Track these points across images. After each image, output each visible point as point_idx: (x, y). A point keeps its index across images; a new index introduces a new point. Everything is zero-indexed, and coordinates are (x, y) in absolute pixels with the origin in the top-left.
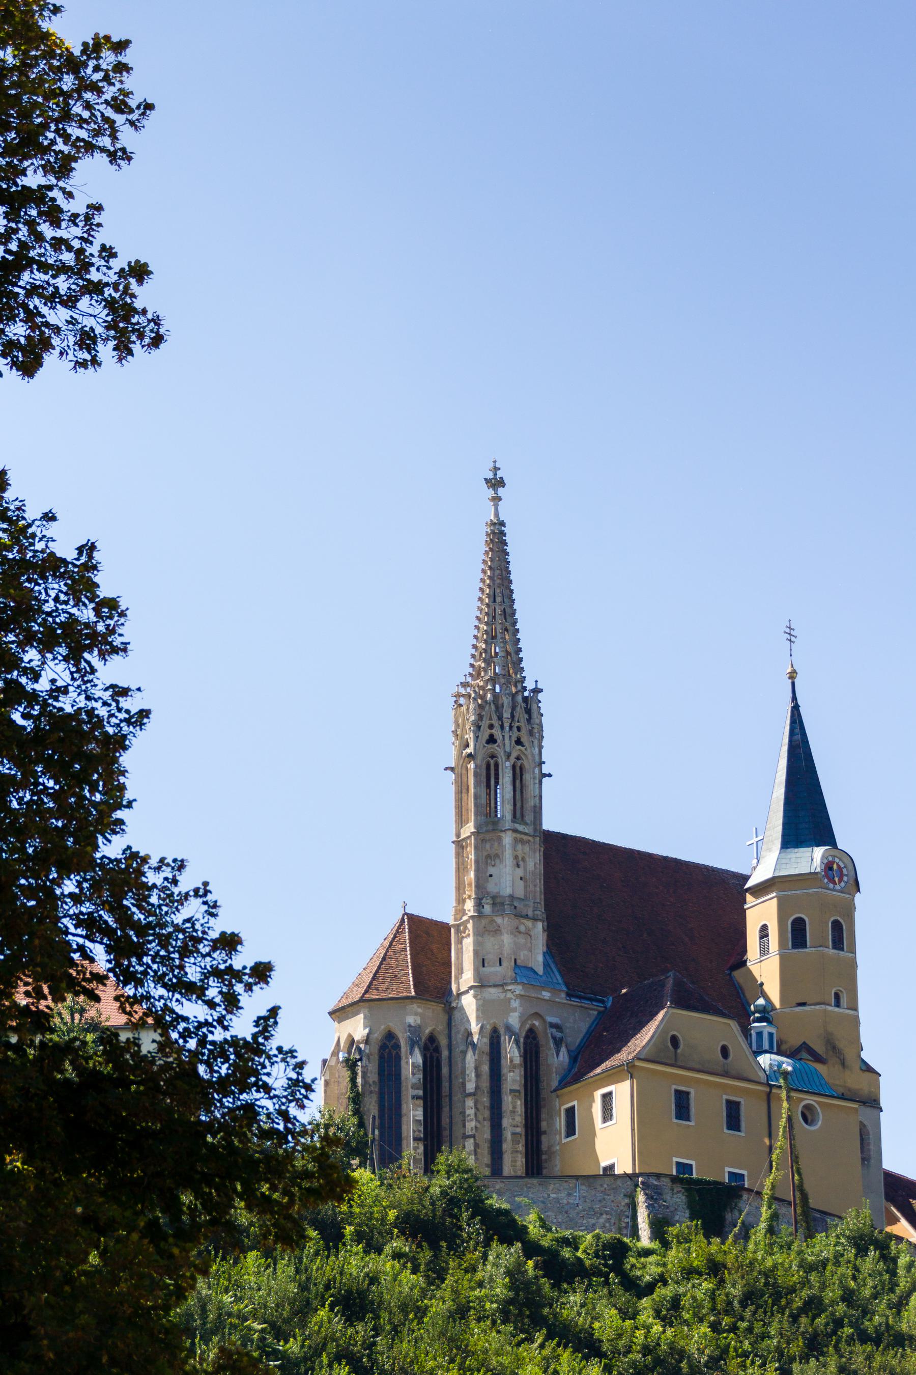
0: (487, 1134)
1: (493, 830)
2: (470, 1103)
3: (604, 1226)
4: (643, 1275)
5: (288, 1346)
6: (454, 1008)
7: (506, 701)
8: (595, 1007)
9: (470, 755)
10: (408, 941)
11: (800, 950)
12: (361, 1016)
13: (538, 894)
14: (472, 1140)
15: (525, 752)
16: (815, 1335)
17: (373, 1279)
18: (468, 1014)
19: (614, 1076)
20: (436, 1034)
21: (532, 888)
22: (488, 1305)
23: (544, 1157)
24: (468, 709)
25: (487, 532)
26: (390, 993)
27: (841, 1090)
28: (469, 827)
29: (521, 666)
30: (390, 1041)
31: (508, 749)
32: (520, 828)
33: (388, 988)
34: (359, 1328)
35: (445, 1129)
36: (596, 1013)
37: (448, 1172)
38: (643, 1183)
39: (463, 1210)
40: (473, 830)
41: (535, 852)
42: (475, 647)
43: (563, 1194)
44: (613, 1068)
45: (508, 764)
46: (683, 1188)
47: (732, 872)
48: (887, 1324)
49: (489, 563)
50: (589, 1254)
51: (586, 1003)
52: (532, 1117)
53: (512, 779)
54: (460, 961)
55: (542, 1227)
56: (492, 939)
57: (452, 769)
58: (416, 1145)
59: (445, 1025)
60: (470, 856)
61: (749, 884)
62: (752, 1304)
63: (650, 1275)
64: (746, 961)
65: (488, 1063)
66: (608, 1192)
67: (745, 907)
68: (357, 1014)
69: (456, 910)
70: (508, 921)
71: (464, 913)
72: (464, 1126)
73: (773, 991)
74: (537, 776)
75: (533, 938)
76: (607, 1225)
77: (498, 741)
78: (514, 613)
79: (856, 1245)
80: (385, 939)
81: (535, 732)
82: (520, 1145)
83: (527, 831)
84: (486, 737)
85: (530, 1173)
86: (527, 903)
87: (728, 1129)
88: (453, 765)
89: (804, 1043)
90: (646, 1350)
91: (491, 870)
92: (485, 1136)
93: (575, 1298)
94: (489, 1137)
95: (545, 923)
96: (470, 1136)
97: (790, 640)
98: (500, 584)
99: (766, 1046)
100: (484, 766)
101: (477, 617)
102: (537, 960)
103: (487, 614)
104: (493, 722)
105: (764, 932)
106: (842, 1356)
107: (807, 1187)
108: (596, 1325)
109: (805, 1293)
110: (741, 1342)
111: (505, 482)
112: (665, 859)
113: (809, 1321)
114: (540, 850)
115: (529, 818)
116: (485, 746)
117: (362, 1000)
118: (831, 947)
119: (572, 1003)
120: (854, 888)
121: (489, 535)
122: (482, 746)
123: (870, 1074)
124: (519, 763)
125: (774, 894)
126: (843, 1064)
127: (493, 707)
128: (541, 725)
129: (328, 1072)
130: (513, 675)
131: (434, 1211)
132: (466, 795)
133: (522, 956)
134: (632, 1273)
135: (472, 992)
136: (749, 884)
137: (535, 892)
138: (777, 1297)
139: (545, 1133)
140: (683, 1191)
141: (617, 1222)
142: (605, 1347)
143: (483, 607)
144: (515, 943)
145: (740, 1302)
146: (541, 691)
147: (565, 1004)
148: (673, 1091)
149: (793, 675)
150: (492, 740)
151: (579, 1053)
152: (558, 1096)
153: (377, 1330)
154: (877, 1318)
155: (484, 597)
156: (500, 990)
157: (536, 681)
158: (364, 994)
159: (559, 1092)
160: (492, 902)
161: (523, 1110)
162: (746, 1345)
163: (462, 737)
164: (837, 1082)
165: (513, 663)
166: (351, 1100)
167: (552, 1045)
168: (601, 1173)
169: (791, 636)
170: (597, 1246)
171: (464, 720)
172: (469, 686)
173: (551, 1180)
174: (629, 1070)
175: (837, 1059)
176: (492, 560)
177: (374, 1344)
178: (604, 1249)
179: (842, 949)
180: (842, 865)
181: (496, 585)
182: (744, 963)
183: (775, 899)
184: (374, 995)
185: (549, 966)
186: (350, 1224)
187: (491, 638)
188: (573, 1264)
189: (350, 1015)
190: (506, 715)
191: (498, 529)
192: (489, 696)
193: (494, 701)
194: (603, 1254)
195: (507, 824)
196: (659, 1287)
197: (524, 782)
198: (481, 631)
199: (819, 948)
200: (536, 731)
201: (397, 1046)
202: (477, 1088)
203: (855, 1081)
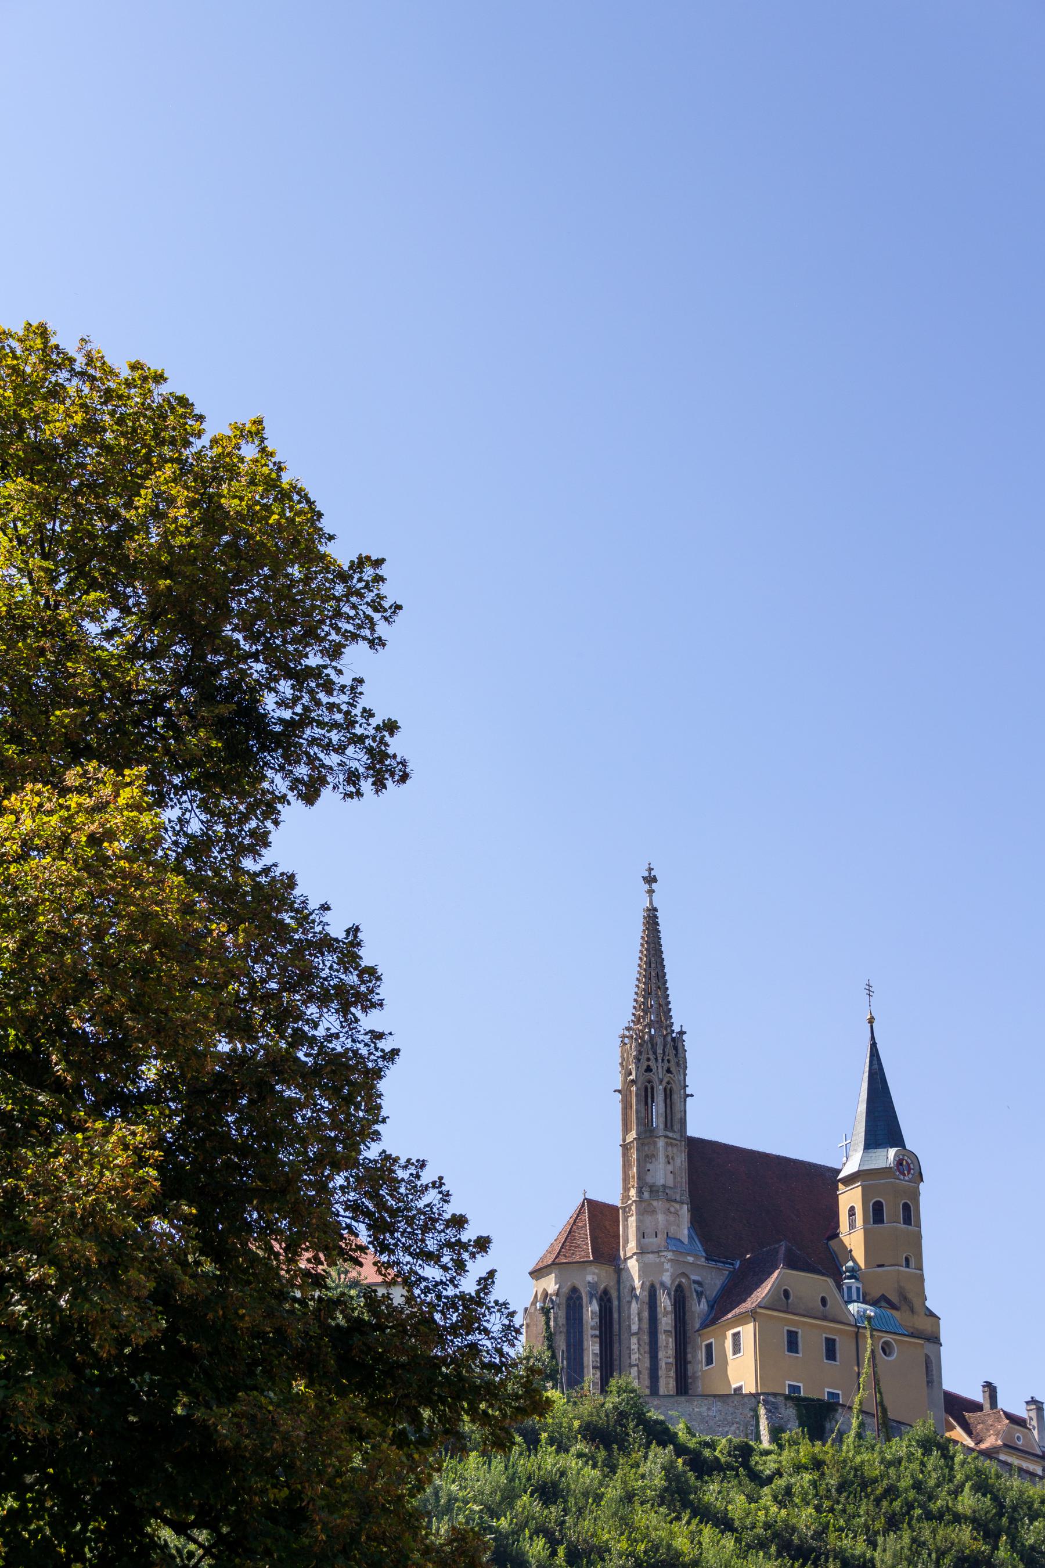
0: (647, 1364)
7: (659, 1041)
9: (632, 1081)
16: (894, 1514)
17: (563, 1474)
19: (741, 1320)
21: (679, 1179)
32: (670, 1134)
34: (553, 1510)
37: (618, 1392)
42: (635, 1000)
43: (704, 1409)
44: (741, 1314)
48: (947, 1507)
57: (619, 1091)
61: (841, 1176)
71: (629, 1199)
78: (664, 975)
81: (681, 1064)
84: (645, 1067)
88: (620, 1088)
90: (767, 1526)
93: (714, 1487)
96: (634, 1365)
99: (855, 1297)
102: (684, 1232)
103: (645, 976)
105: (852, 1211)
107: (886, 1403)
108: (730, 1507)
115: (677, 1127)
117: (554, 1263)
123: (930, 1318)
126: (912, 1311)
131: (608, 1421)
133: (673, 1229)
136: (841, 1176)
138: (864, 1485)
149: (871, 1021)
150: (649, 1069)
154: (939, 1503)
156: (656, 1255)
162: (842, 1522)
165: (664, 1012)
173: (696, 1399)
174: (753, 1315)
176: (647, 936)
177: (564, 1522)
182: (837, 1235)
186: (545, 1432)
187: (647, 994)
188: (711, 1461)
190: (659, 1051)
201: (580, 1298)
202: (639, 1329)
203: (922, 1323)
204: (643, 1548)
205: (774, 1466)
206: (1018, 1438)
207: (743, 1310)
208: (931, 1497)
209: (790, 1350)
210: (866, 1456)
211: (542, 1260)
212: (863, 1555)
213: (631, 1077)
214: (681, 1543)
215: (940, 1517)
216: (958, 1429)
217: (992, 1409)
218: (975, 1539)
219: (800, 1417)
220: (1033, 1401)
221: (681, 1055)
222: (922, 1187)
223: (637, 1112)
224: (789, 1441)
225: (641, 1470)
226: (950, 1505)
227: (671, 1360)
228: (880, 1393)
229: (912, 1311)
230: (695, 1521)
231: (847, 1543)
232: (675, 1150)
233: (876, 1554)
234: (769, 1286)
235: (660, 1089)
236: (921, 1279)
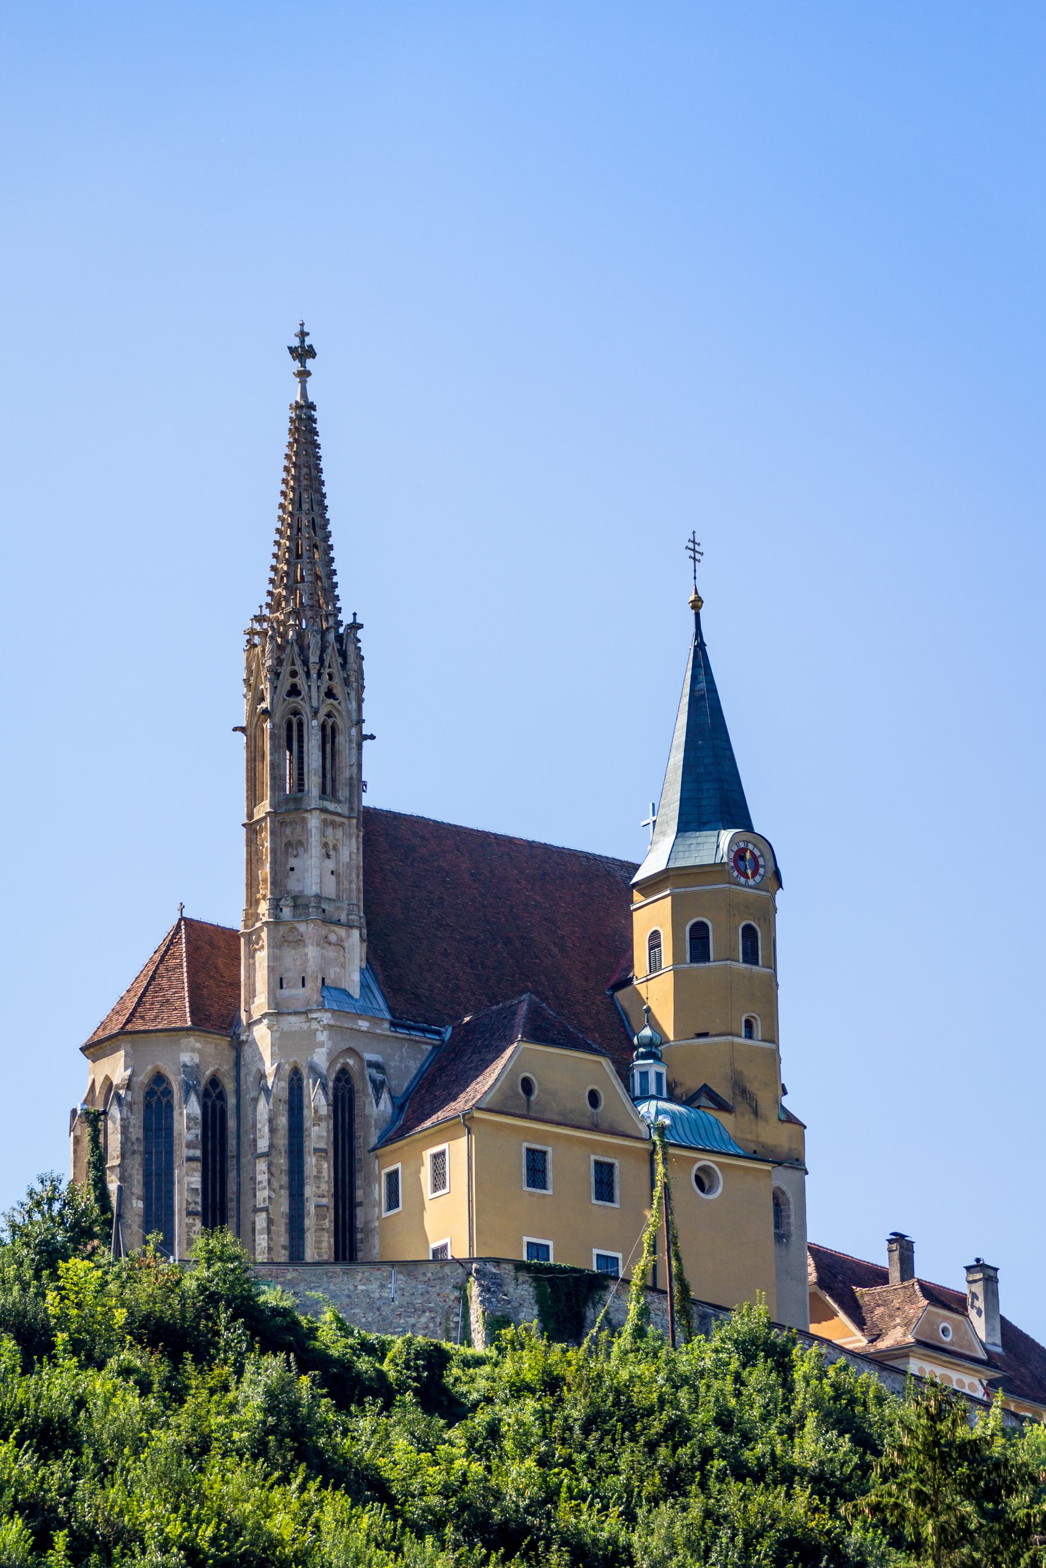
0: (284, 1206)
1: (296, 809)
2: (262, 1166)
3: (427, 1327)
4: (469, 1392)
6: (243, 1042)
7: (313, 641)
8: (429, 1041)
9: (265, 712)
10: (184, 955)
11: (701, 965)
12: (122, 1053)
13: (354, 894)
14: (264, 1215)
15: (339, 707)
16: (679, 1468)
17: (81, 1403)
18: (261, 1050)
19: (446, 1130)
20: (219, 1076)
21: (346, 885)
22: (236, 1436)
23: (359, 1236)
24: (263, 651)
25: (291, 418)
26: (159, 1022)
27: (753, 1147)
28: (264, 806)
29: (336, 593)
30: (159, 1085)
31: (315, 704)
32: (331, 806)
33: (156, 1017)
34: (55, 1468)
35: (232, 1200)
36: (430, 1048)
37: (208, 1260)
39: (222, 1308)
40: (269, 810)
42: (274, 568)
43: (374, 1286)
44: (447, 1120)
46: (530, 1277)
47: (621, 861)
48: (773, 1454)
50: (397, 1365)
51: (416, 1035)
52: (344, 1186)
53: (320, 742)
54: (251, 980)
55: (340, 1329)
56: (293, 952)
57: (243, 730)
58: (191, 1221)
59: (232, 1063)
60: (266, 844)
61: (638, 877)
62: (598, 1429)
63: (478, 1392)
64: (633, 978)
65: (286, 1115)
66: (432, 1283)
67: (632, 908)
68: (118, 1050)
70: (314, 929)
71: (258, 919)
72: (255, 1196)
74: (354, 738)
75: (346, 950)
76: (431, 1325)
77: (303, 693)
79: (745, 1352)
80: (155, 952)
81: (354, 682)
82: (327, 1220)
83: (340, 811)
84: (287, 687)
85: (341, 1257)
87: (597, 1199)
88: (244, 724)
89: (705, 1085)
90: (447, 1491)
91: (292, 862)
92: (282, 1210)
93: (365, 1424)
94: (287, 1210)
95: (365, 931)
96: (262, 1210)
97: (694, 559)
98: (307, 486)
99: (653, 1090)
100: (284, 726)
102: (353, 979)
103: (290, 526)
104: (296, 668)
106: (709, 1497)
107: (687, 1276)
109: (668, 1414)
110: (577, 1480)
111: (316, 351)
112: (531, 845)
113: (670, 1452)
114: (358, 837)
115: (343, 793)
117: (123, 1032)
118: (741, 961)
119: (398, 1035)
120: (773, 883)
122: (281, 699)
123: (791, 1126)
124: (330, 721)
126: (756, 1113)
127: (296, 648)
128: (360, 672)
130: (324, 607)
131: (183, 1311)
132: (261, 764)
133: (333, 974)
134: (456, 1389)
135: (265, 1021)
136: (638, 877)
138: (629, 1422)
139: (360, 1204)
140: (530, 1280)
141: (443, 1321)
142: (395, 1489)
143: (286, 516)
144: (323, 957)
146: (361, 626)
148: (524, 1150)
149: (697, 604)
150: (294, 691)
151: (405, 1102)
152: (377, 1157)
153: (77, 1472)
154: (760, 1448)
155: (286, 503)
156: (303, 1018)
157: (355, 614)
158: (126, 1024)
159: (379, 1152)
160: (292, 904)
161: (332, 1175)
162: (585, 1484)
163: (256, 687)
164: (748, 1137)
165: (324, 590)
166: (92, 1165)
167: (370, 1090)
168: (431, 1258)
169: (695, 552)
170: (408, 1354)
171: (258, 666)
172: (265, 621)
174: (467, 1122)
175: (748, 1107)
176: (296, 454)
177: (73, 1489)
178: (417, 1358)
179: (756, 963)
180: (757, 853)
181: (303, 487)
182: (628, 982)
184: (138, 1025)
185: (369, 987)
186: (62, 1331)
187: (295, 555)
189: (108, 1052)
190: (314, 658)
191: (305, 414)
193: (297, 641)
194: (415, 1364)
195: (313, 802)
196: (482, 1408)
197: (337, 747)
198: (283, 548)
199: (725, 962)
200: (353, 679)
201: (168, 1092)
202: (271, 1146)
203: (773, 1135)
204: (209, 1533)
205: (482, 1384)
208: (747, 1439)
210: (644, 1369)
211: (103, 1025)
212: (613, 1540)
213: (264, 705)
215: (758, 1477)
216: (842, 1316)
217: (903, 1280)
219: (540, 1300)
220: (979, 1266)
221: (352, 664)
222: (781, 897)
224: (512, 1342)
226: (779, 1450)
228: (678, 1259)
229: (756, 1113)
230: (313, 1486)
231: (587, 1519)
232: (339, 833)
233: (635, 1538)
235: (314, 725)
236: (774, 1059)
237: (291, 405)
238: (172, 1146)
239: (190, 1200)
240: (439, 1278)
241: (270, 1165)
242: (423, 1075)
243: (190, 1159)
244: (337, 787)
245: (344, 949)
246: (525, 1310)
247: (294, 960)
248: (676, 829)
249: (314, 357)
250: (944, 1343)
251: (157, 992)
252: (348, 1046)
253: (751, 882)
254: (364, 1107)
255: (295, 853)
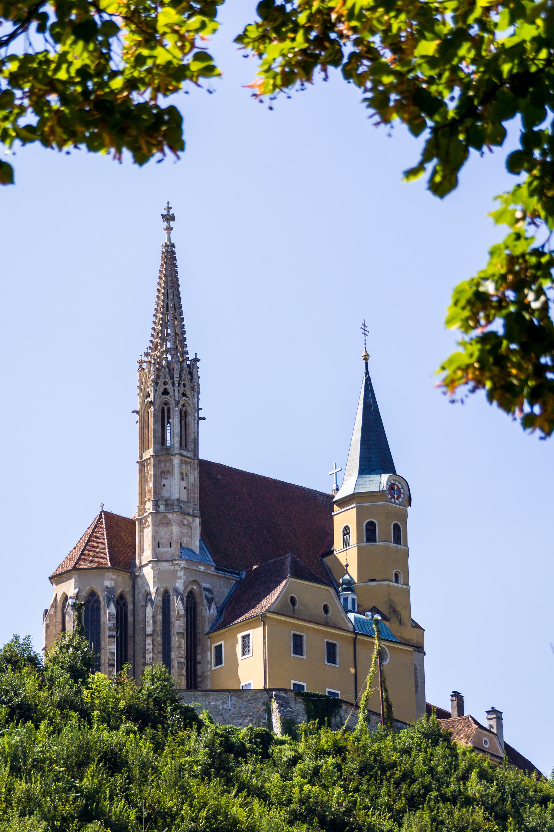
1: (167, 454)
2: (149, 641)
5: (82, 783)
7: (176, 366)
9: (151, 402)
10: (105, 530)
12: (73, 580)
15: (189, 402)
19: (252, 623)
20: (124, 593)
21: (192, 495)
22: (195, 768)
23: (199, 680)
24: (149, 371)
25: (162, 251)
29: (185, 343)
31: (177, 399)
32: (185, 453)
36: (234, 582)
37: (152, 680)
38: (275, 695)
39: (168, 704)
40: (152, 454)
41: (194, 471)
42: (153, 329)
43: (219, 703)
44: (251, 618)
45: (177, 409)
46: (302, 699)
49: (164, 272)
51: (228, 575)
56: (165, 529)
57: (137, 412)
58: (111, 669)
60: (150, 472)
61: (334, 500)
62: (366, 774)
63: (287, 757)
65: (161, 614)
68: (70, 578)
69: (139, 509)
71: (145, 511)
72: (144, 657)
73: (353, 572)
77: (170, 393)
78: (181, 307)
80: (88, 528)
81: (195, 388)
84: (162, 390)
86: (189, 505)
88: (138, 410)
89: (374, 607)
90: (302, 802)
91: (164, 482)
97: (365, 334)
99: (350, 607)
100: (160, 410)
101: (155, 309)
102: (196, 544)
104: (167, 380)
105: (346, 532)
107: (391, 700)
108: (267, 785)
112: (276, 481)
115: (190, 446)
116: (161, 397)
117: (74, 569)
120: (407, 503)
121: (164, 253)
124: (184, 409)
125: (354, 505)
126: (400, 622)
127: (167, 370)
128: (198, 384)
129: (48, 619)
133: (186, 540)
135: (150, 565)
136: (334, 500)
137: (194, 498)
139: (200, 663)
140: (303, 701)
141: (257, 722)
143: (160, 302)
144: (181, 532)
145: (358, 773)
146: (199, 360)
147: (214, 575)
148: (292, 635)
149: (366, 358)
150: (166, 392)
151: (223, 609)
152: (209, 638)
156: (170, 563)
157: (196, 354)
159: (211, 635)
163: (145, 390)
165: (180, 341)
167: (205, 603)
170: (251, 735)
171: (146, 379)
173: (211, 693)
174: (263, 619)
176: (166, 270)
178: (256, 738)
179: (400, 544)
180: (400, 487)
182: (332, 552)
183: (355, 508)
184: (82, 565)
188: (238, 747)
189: (65, 580)
190: (176, 375)
192: (164, 362)
193: (167, 366)
195: (176, 451)
200: (196, 387)
201: (98, 601)
202: (154, 630)
203: (409, 634)
206: (485, 741)
207: (253, 614)
209: (295, 652)
211: (61, 566)
213: (149, 399)
214: (236, 811)
215: (454, 800)
218: (488, 819)
223: (155, 431)
224: (305, 731)
225: (187, 748)
227: (183, 660)
228: (386, 690)
232: (189, 468)
234: (278, 593)
236: (407, 593)
237: (162, 245)
238: (99, 630)
239: (110, 658)
240: (255, 699)
241: (153, 641)
242: (232, 595)
243: (110, 637)
244: (187, 443)
245: (191, 528)
246: (300, 717)
247: (166, 533)
248: (357, 472)
249: (174, 221)
250: (485, 748)
251: (91, 549)
252: (193, 579)
253: (397, 501)
254: (202, 611)
255: (166, 477)
